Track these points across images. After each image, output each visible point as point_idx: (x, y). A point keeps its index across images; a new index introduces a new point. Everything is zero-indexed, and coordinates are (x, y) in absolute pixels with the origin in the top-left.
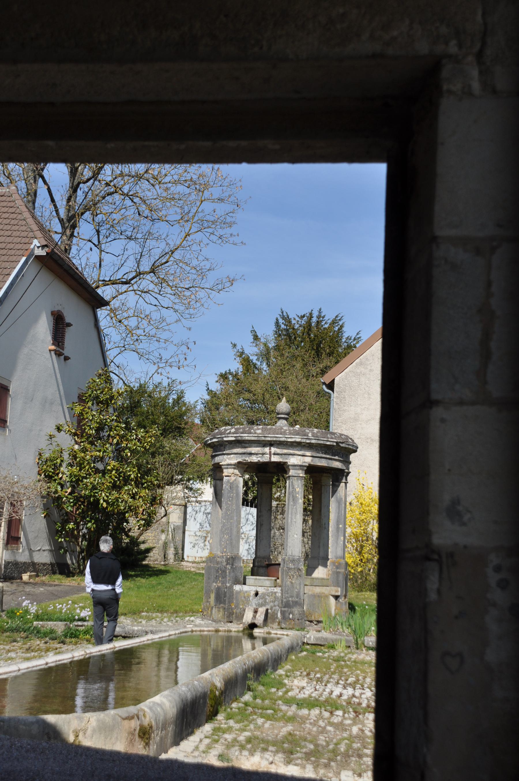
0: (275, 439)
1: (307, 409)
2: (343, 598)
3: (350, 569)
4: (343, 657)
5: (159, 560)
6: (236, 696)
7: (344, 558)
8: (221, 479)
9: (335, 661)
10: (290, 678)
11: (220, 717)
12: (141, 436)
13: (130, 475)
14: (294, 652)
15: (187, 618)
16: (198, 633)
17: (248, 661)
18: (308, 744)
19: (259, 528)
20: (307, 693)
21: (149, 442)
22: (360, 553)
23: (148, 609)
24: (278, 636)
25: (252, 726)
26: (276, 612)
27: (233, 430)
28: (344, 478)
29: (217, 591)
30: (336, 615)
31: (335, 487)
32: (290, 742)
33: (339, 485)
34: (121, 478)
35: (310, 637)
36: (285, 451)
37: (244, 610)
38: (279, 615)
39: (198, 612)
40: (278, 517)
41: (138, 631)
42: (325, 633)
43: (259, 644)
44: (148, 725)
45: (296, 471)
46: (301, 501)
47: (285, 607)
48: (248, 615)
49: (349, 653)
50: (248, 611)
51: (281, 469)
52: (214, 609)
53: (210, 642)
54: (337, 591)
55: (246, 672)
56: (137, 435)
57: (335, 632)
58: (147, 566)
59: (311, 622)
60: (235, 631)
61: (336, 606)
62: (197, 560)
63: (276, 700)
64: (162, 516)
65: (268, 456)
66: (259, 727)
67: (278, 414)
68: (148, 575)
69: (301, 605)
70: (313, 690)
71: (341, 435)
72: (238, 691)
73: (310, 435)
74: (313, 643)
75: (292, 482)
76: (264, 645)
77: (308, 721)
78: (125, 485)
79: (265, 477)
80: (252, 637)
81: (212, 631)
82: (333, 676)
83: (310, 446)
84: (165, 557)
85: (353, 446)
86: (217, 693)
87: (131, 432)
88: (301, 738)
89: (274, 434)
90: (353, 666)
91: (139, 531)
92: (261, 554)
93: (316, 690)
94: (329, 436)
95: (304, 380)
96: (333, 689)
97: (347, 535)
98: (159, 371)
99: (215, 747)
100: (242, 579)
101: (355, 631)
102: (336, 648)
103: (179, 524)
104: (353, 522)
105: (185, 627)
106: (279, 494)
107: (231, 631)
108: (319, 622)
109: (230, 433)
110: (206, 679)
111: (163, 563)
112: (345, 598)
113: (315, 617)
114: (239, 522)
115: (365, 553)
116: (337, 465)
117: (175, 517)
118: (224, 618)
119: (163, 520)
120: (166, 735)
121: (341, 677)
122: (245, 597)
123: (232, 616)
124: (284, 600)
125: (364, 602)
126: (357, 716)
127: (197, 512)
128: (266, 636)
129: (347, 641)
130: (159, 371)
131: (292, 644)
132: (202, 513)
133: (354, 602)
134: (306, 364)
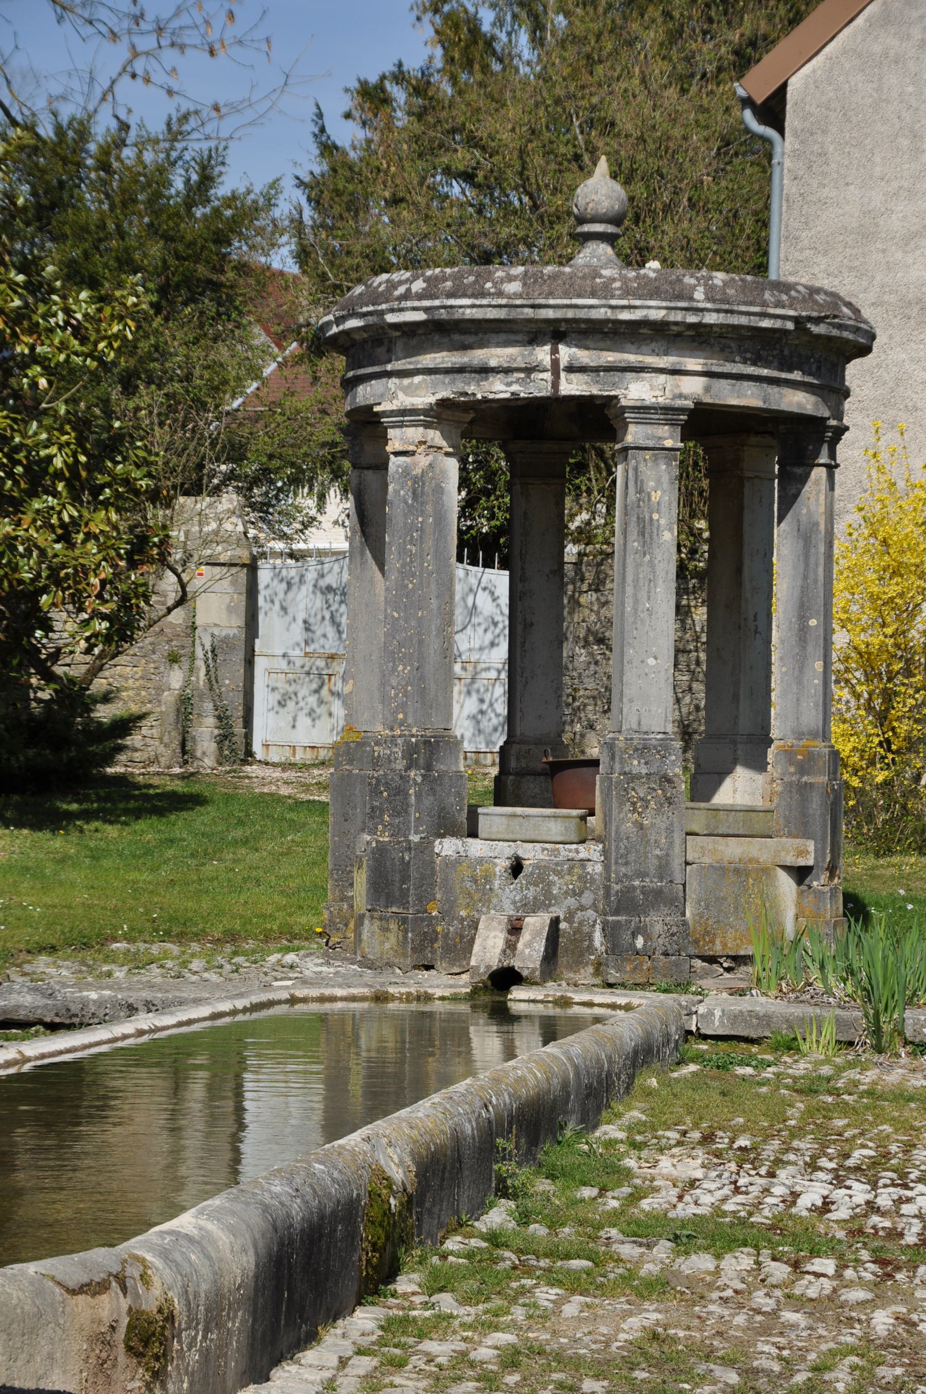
0: (570, 314)
1: (685, 201)
2: (824, 877)
3: (846, 776)
4: (829, 1080)
5: (162, 760)
6: (457, 1213)
7: (825, 735)
8: (382, 466)
9: (799, 1091)
10: (644, 1154)
11: (405, 1284)
12: (86, 315)
13: (50, 458)
14: (656, 1065)
15: (273, 958)
16: (314, 1007)
17: (498, 1095)
18: (719, 1371)
19: (519, 640)
20: (706, 1200)
21: (116, 336)
22: (882, 718)
23: (132, 929)
24: (597, 1011)
25: (519, 1313)
26: (586, 929)
27: (418, 286)
28: (825, 448)
29: (376, 860)
30: (799, 935)
31: (792, 484)
32: (656, 1364)
33: (808, 475)
34: (19, 470)
35: (711, 1013)
36: (610, 358)
37: (475, 925)
39: (308, 935)
40: (583, 600)
41: (100, 1003)
42: (763, 999)
43: (528, 1040)
44: (160, 1311)
45: (650, 429)
46: (669, 537)
47: (617, 912)
48: (490, 942)
49: (851, 1065)
50: (487, 928)
51: (597, 421)
52: (366, 922)
53: (357, 1037)
54: (802, 853)
55: (490, 1132)
56: (68, 311)
57: (801, 991)
58: (122, 780)
59: (712, 960)
60: (442, 998)
61: (799, 904)
62: (299, 757)
63: (600, 1227)
64: (170, 603)
65: (547, 376)
66: (545, 1317)
67: (581, 220)
68: (126, 812)
70: (727, 1191)
71: (813, 291)
72: (465, 1195)
73: (699, 294)
74: (720, 1032)
75: (636, 469)
76: (545, 1043)
77: (715, 1295)
78: (33, 493)
79: (534, 463)
80: (502, 1015)
81: (363, 999)
82: (796, 1143)
83: (697, 338)
84: (185, 750)
85: (857, 330)
86: (392, 1201)
87: (45, 301)
88: (691, 1349)
89: (567, 295)
90: (867, 1108)
91: (88, 658)
92: (529, 727)
93: (737, 1190)
94: (767, 295)
95: (672, 92)
96: (798, 1189)
97: (834, 657)
98: (139, 66)
99: (392, 1385)
100: (463, 817)
101: (868, 994)
102: (804, 1047)
103: (232, 632)
104: (854, 608)
105: (267, 986)
106: (585, 516)
107: (428, 998)
108: (740, 960)
109: (407, 296)
110: (353, 1153)
111: (177, 770)
112: (831, 877)
113: (724, 945)
114: (449, 621)
115: (899, 719)
116: (799, 404)
117: (216, 608)
118: (405, 955)
119: (171, 618)
120: (223, 1345)
121: (824, 1146)
123: (432, 945)
125: (902, 892)
126: (890, 1276)
127: (289, 585)
128: (552, 1011)
129: (840, 1023)
130: (139, 66)
131: (648, 1035)
132: (307, 589)
133: (863, 891)
134: (680, 32)
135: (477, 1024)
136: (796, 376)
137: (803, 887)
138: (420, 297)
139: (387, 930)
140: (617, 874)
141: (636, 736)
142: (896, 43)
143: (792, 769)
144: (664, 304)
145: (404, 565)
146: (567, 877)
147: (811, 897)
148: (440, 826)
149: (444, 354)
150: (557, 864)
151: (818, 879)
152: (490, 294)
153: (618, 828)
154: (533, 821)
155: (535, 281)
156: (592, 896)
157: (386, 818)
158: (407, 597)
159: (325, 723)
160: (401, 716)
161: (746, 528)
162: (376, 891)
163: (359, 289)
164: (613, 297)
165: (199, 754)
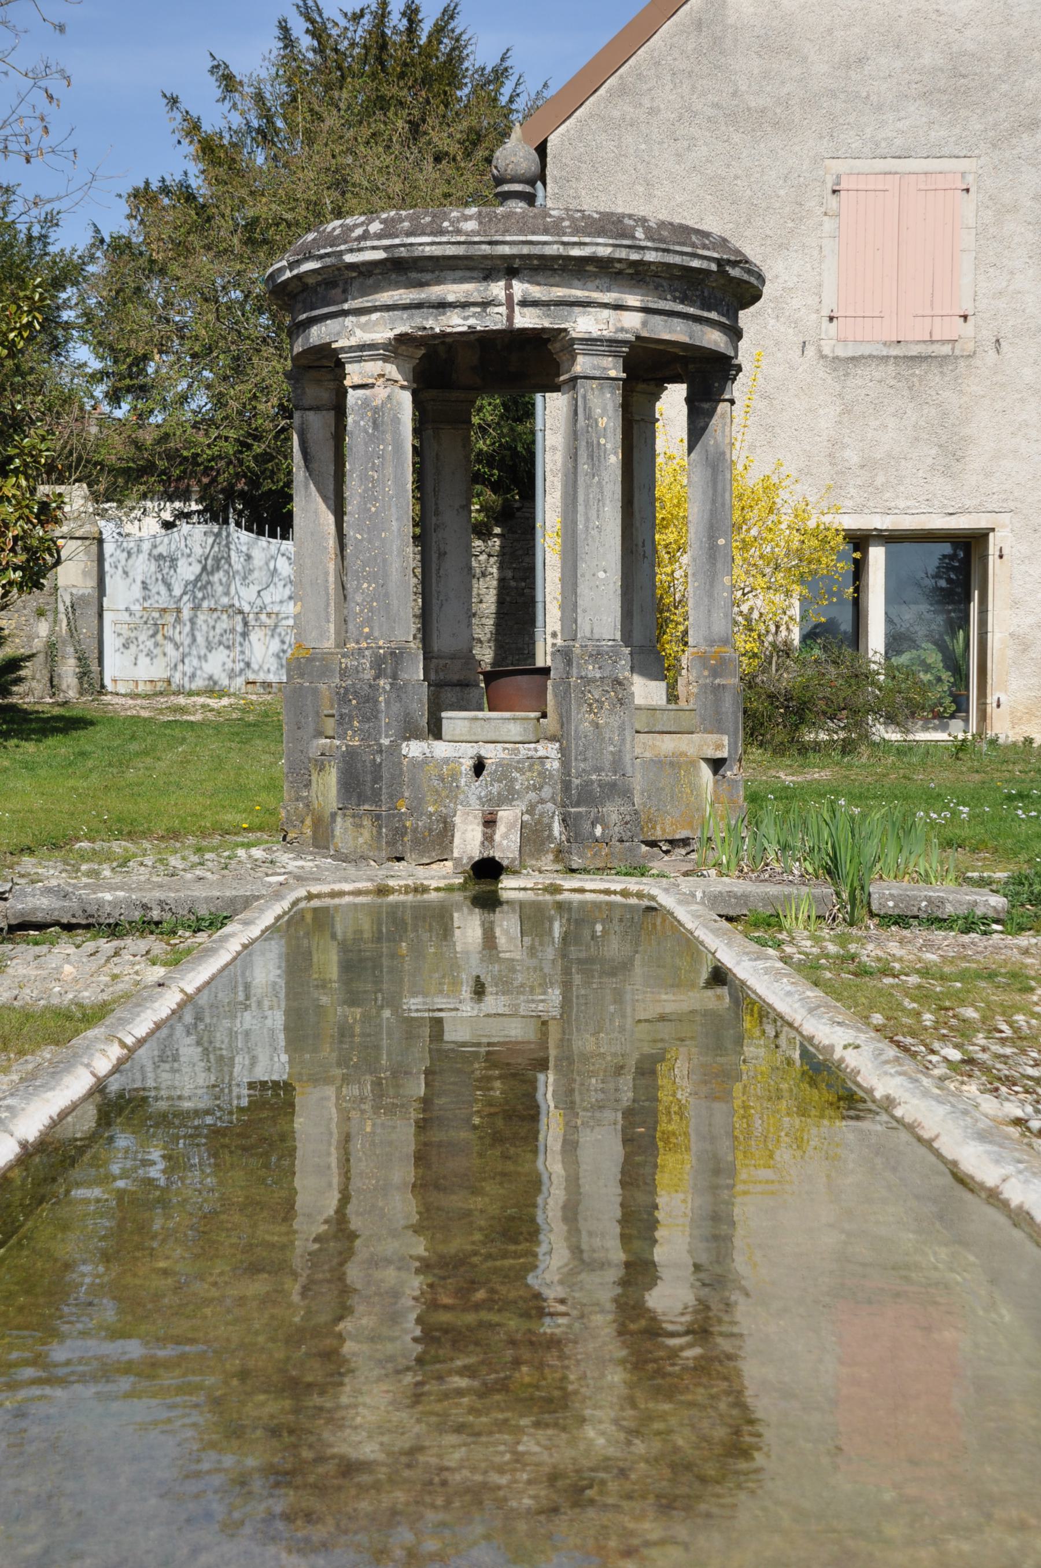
0: (525, 250)
26: (546, 820)
27: (375, 227)
33: (714, 410)
36: (559, 292)
38: (557, 828)
41: (115, 904)
45: (596, 360)
47: (578, 804)
48: (469, 835)
52: (339, 819)
54: (719, 747)
59: (653, 844)
60: (438, 889)
62: (141, 688)
65: (503, 310)
69: (626, 794)
75: (584, 397)
81: (367, 892)
84: (53, 684)
89: (521, 232)
103: (87, 591)
107: (425, 890)
109: (366, 236)
116: (716, 342)
118: (380, 849)
122: (442, 779)
124: (576, 782)
127: (129, 554)
132: (143, 556)
136: (713, 315)
137: (718, 777)
138: (379, 236)
139: (361, 826)
140: (577, 769)
143: (706, 673)
144: (611, 241)
145: (365, 491)
146: (528, 774)
149: (402, 291)
150: (518, 762)
151: (731, 770)
154: (493, 723)
155: (490, 220)
157: (356, 724)
158: (370, 520)
159: (161, 661)
160: (367, 630)
161: (636, 465)
162: (347, 790)
163: (311, 236)
164: (564, 234)
165: (64, 687)
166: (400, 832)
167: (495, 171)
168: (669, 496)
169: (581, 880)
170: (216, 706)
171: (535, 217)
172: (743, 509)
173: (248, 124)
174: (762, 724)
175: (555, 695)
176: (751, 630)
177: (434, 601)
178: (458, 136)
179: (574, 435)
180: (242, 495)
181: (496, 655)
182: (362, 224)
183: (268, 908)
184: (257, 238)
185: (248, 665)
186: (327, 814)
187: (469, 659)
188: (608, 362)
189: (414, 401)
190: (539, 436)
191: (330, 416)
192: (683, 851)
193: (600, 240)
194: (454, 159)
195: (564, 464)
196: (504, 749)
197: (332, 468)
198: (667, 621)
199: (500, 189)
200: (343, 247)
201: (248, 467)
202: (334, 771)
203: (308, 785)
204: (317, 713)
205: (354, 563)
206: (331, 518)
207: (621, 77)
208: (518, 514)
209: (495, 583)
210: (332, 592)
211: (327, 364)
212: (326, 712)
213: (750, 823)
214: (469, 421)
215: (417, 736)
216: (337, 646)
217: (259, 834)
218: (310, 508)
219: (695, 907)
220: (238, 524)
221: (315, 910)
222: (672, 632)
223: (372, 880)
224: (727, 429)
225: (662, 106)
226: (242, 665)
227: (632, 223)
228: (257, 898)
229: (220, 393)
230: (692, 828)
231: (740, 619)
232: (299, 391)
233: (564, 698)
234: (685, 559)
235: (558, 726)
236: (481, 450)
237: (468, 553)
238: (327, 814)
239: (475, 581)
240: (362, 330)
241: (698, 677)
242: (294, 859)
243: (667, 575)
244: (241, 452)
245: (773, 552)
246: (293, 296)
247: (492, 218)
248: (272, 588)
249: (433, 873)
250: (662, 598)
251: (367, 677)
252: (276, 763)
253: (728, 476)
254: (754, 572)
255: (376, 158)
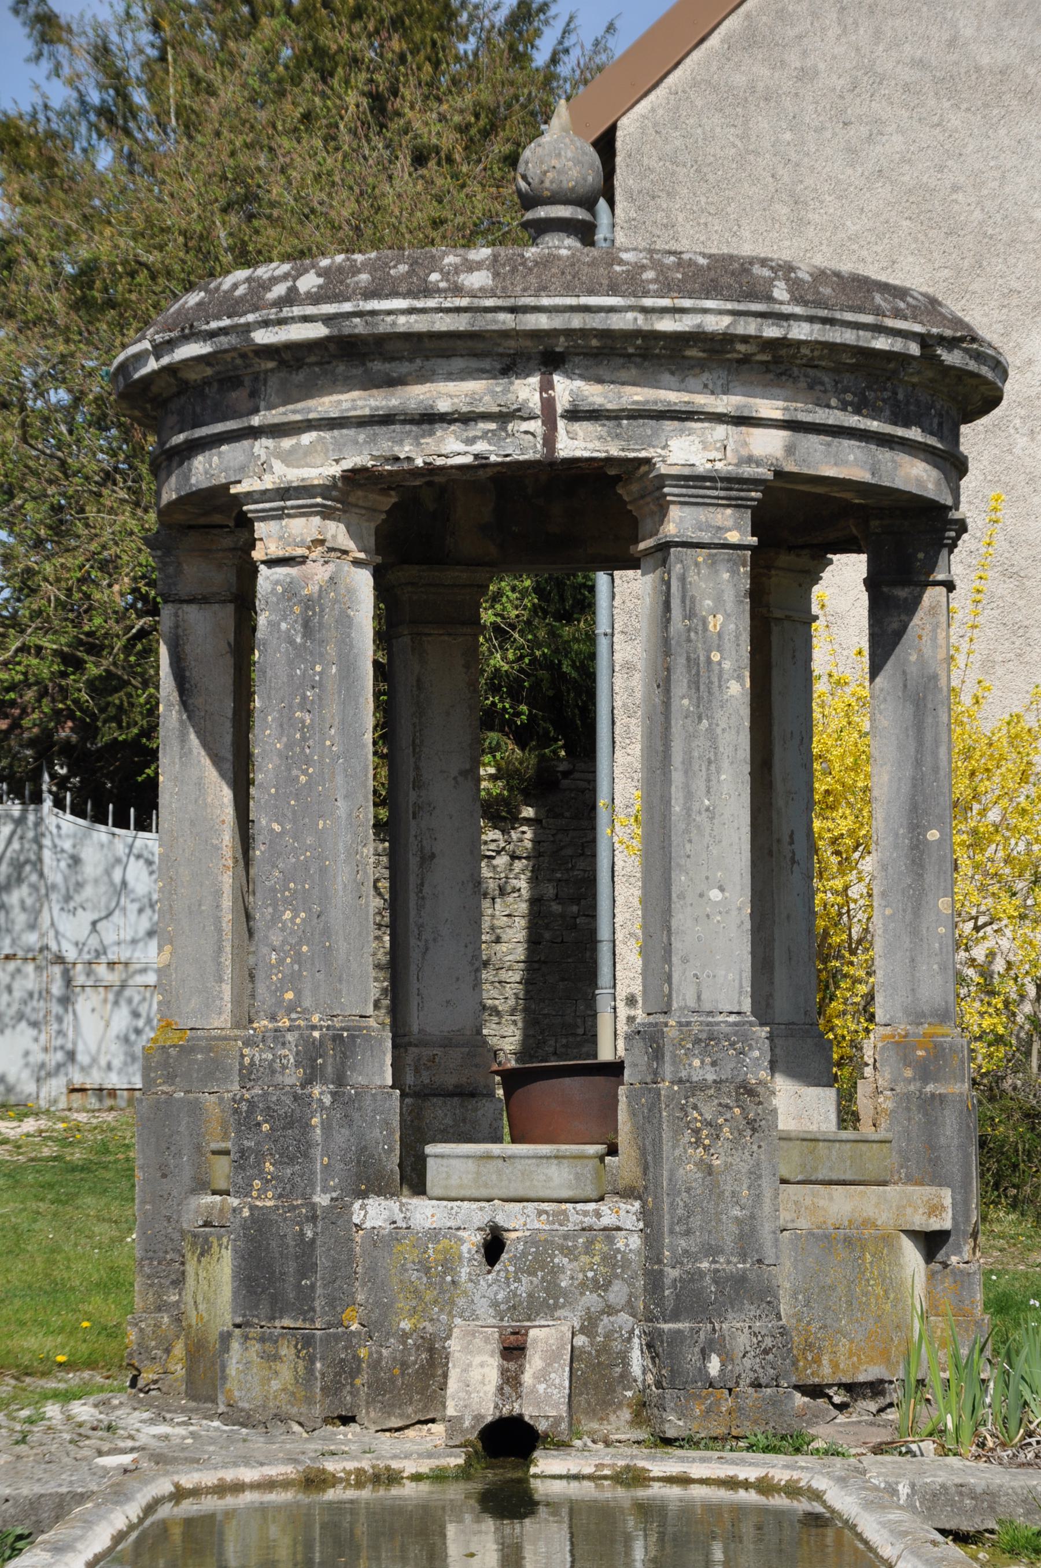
0: (576, 322)
26: (617, 1346)
27: (309, 282)
29: (250, 1239)
33: (917, 601)
36: (637, 395)
45: (703, 514)
47: (675, 1317)
48: (475, 1374)
52: (235, 1345)
54: (935, 1209)
59: (815, 1391)
60: (417, 1478)
65: (536, 426)
69: (765, 1296)
75: (683, 579)
81: (285, 1484)
89: (569, 290)
107: (393, 1478)
109: (292, 298)
116: (919, 481)
118: (309, 1401)
135: (460, 1521)
136: (914, 434)
137: (935, 1266)
138: (315, 299)
139: (276, 1357)
140: (673, 1252)
141: (694, 1018)
142: (766, 72)
143: (909, 1073)
144: (729, 306)
145: (289, 746)
146: (584, 1259)
147: (948, 1282)
148: (359, 1178)
149: (355, 394)
150: (566, 1237)
151: (958, 1251)
152: (439, 291)
153: (672, 1172)
154: (519, 1165)
155: (514, 270)
156: (626, 1289)
157: (269, 1167)
160: (289, 995)
161: (776, 697)
163: (193, 299)
164: (646, 294)
166: (346, 1370)
167: (523, 184)
168: (837, 752)
169: (682, 1460)
170: (12, 1134)
171: (593, 264)
172: (973, 774)
173: (82, 100)
174: (1015, 1167)
175: (633, 1114)
176: (992, 993)
177: (413, 942)
178: (457, 118)
179: (664, 646)
180: (67, 750)
181: (526, 1037)
182: (285, 277)
183: (102, 1518)
184: (95, 297)
185: (71, 1056)
186: (213, 1337)
187: (477, 1046)
188: (725, 517)
189: (378, 587)
190: (603, 644)
191: (227, 614)
192: (873, 1406)
193: (709, 304)
194: (450, 160)
195: (648, 698)
196: (540, 1213)
197: (229, 705)
198: (836, 975)
199: (529, 216)
200: (251, 318)
201: (76, 702)
202: (227, 1255)
203: (179, 1282)
204: (198, 1148)
205: (268, 874)
206: (227, 794)
207: (748, 16)
208: (565, 783)
209: (523, 907)
210: (227, 926)
211: (220, 523)
212: (214, 1146)
213: (996, 1352)
214: (475, 620)
215: (383, 1189)
216: (237, 1025)
217: (86, 1374)
218: (188, 775)
219: (895, 1515)
220: (59, 804)
221: (189, 1523)
222: (846, 996)
223: (295, 1461)
224: (941, 635)
225: (822, 66)
226: (60, 1056)
227: (766, 273)
228: (81, 1498)
229: (28, 570)
230: (888, 1361)
231: (971, 972)
232: (171, 570)
233: (648, 1119)
234: (868, 865)
235: (638, 1171)
236: (497, 670)
237: (475, 855)
238: (213, 1337)
239: (486, 903)
240: (284, 463)
241: (895, 1081)
242: (152, 1422)
243: (836, 893)
244: (64, 675)
245: (1029, 852)
246: (162, 403)
247: (517, 265)
248: (117, 917)
249: (408, 1446)
250: (826, 934)
251: (289, 1081)
252: (122, 1240)
253: (944, 718)
254: (995, 889)
255: (304, 156)
